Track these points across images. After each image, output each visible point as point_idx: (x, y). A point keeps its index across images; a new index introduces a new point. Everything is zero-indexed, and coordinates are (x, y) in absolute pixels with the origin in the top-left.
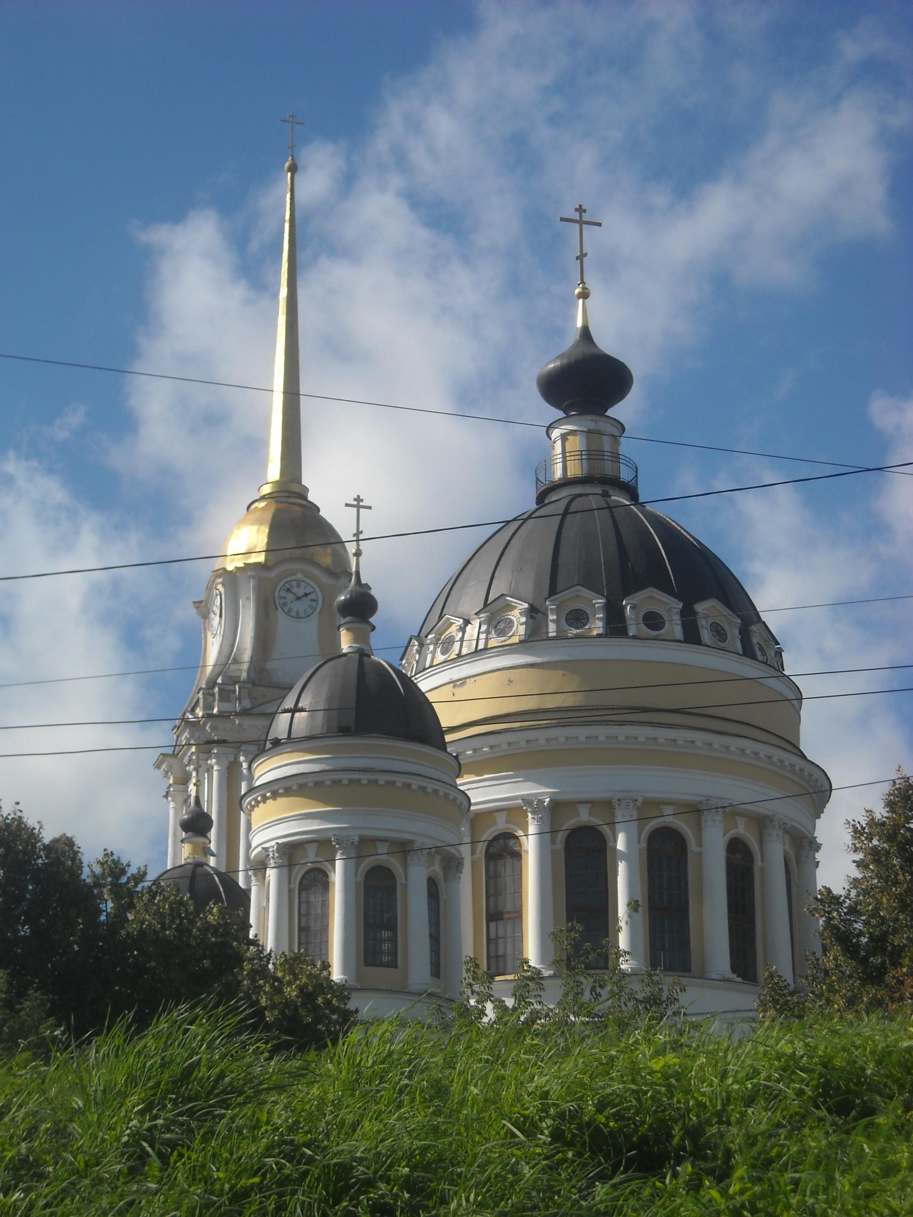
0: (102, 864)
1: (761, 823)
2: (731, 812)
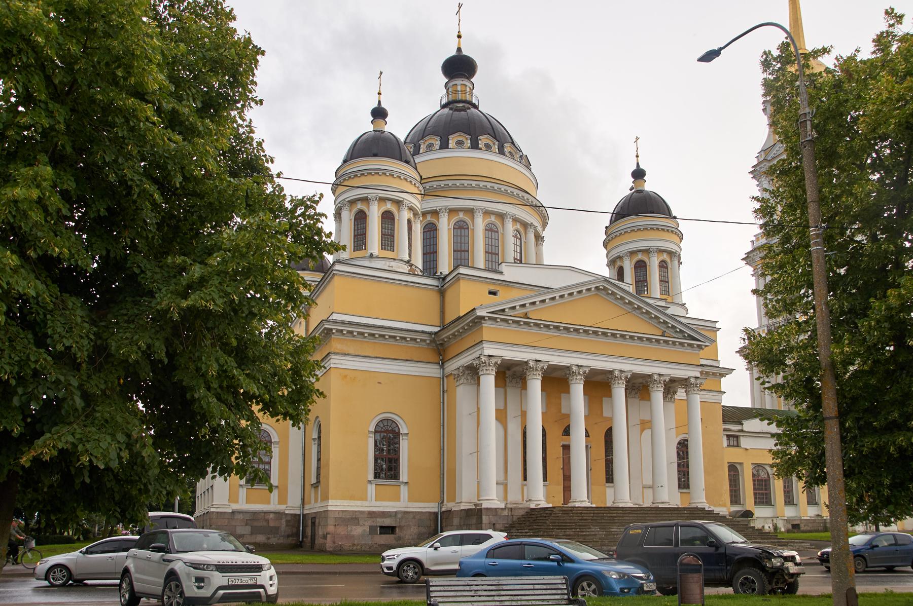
0: (370, 548)
1: (501, 216)
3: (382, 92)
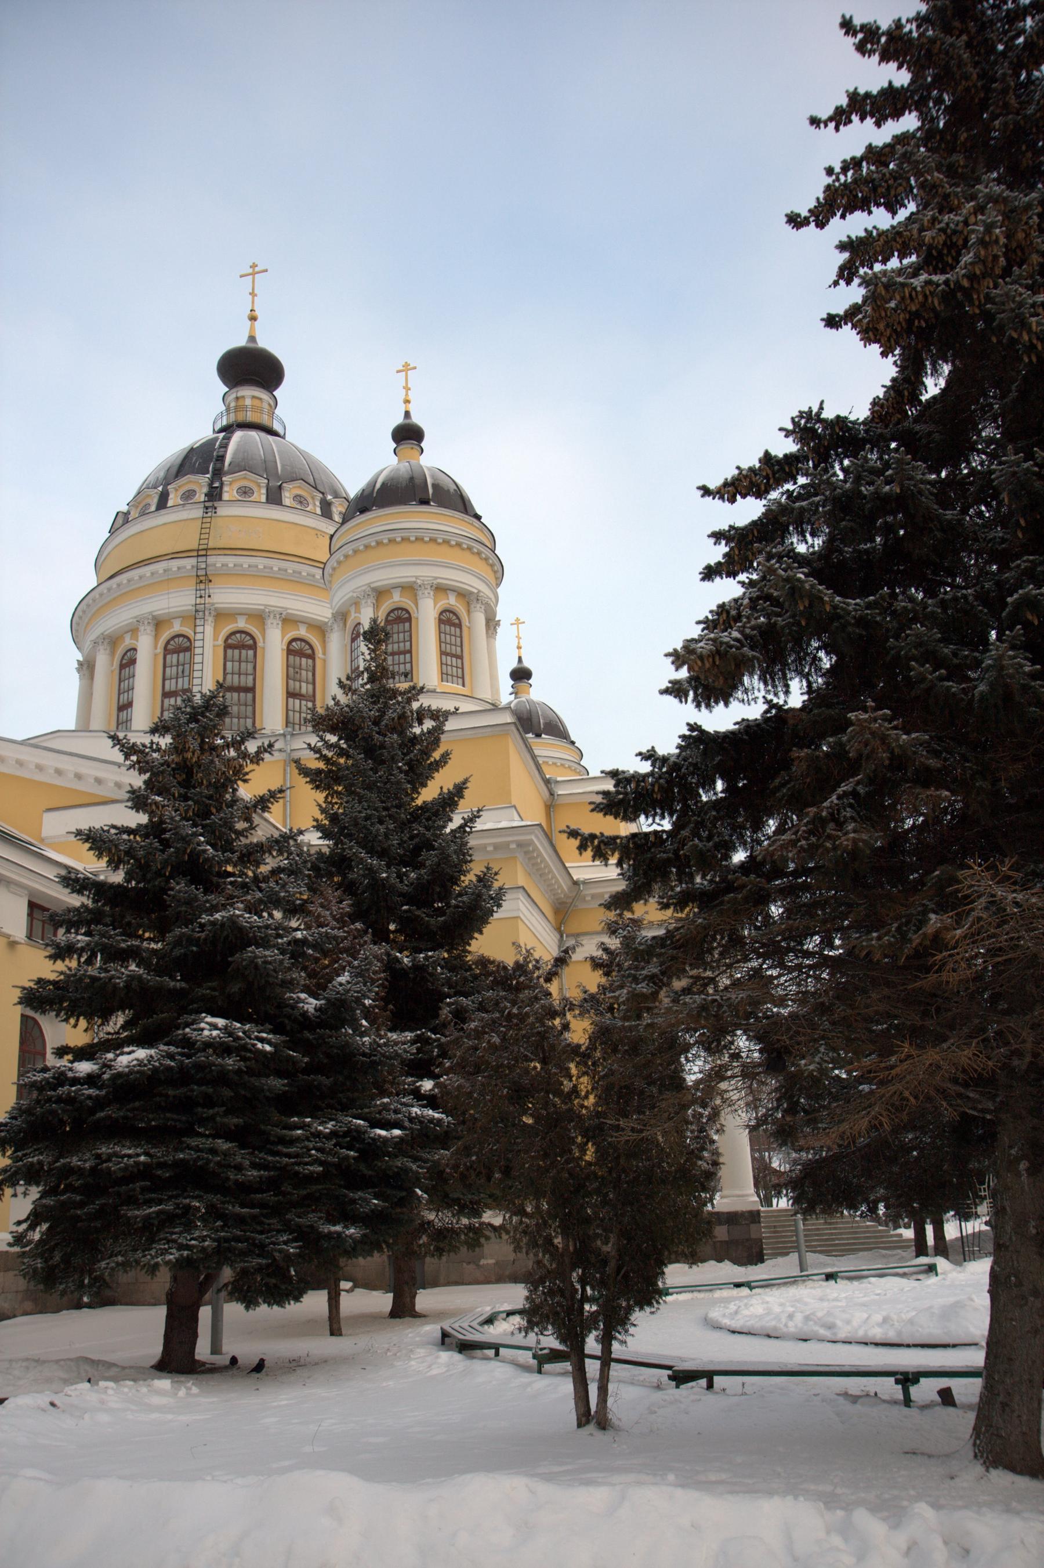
2: (440, 589)
3: (257, 313)
